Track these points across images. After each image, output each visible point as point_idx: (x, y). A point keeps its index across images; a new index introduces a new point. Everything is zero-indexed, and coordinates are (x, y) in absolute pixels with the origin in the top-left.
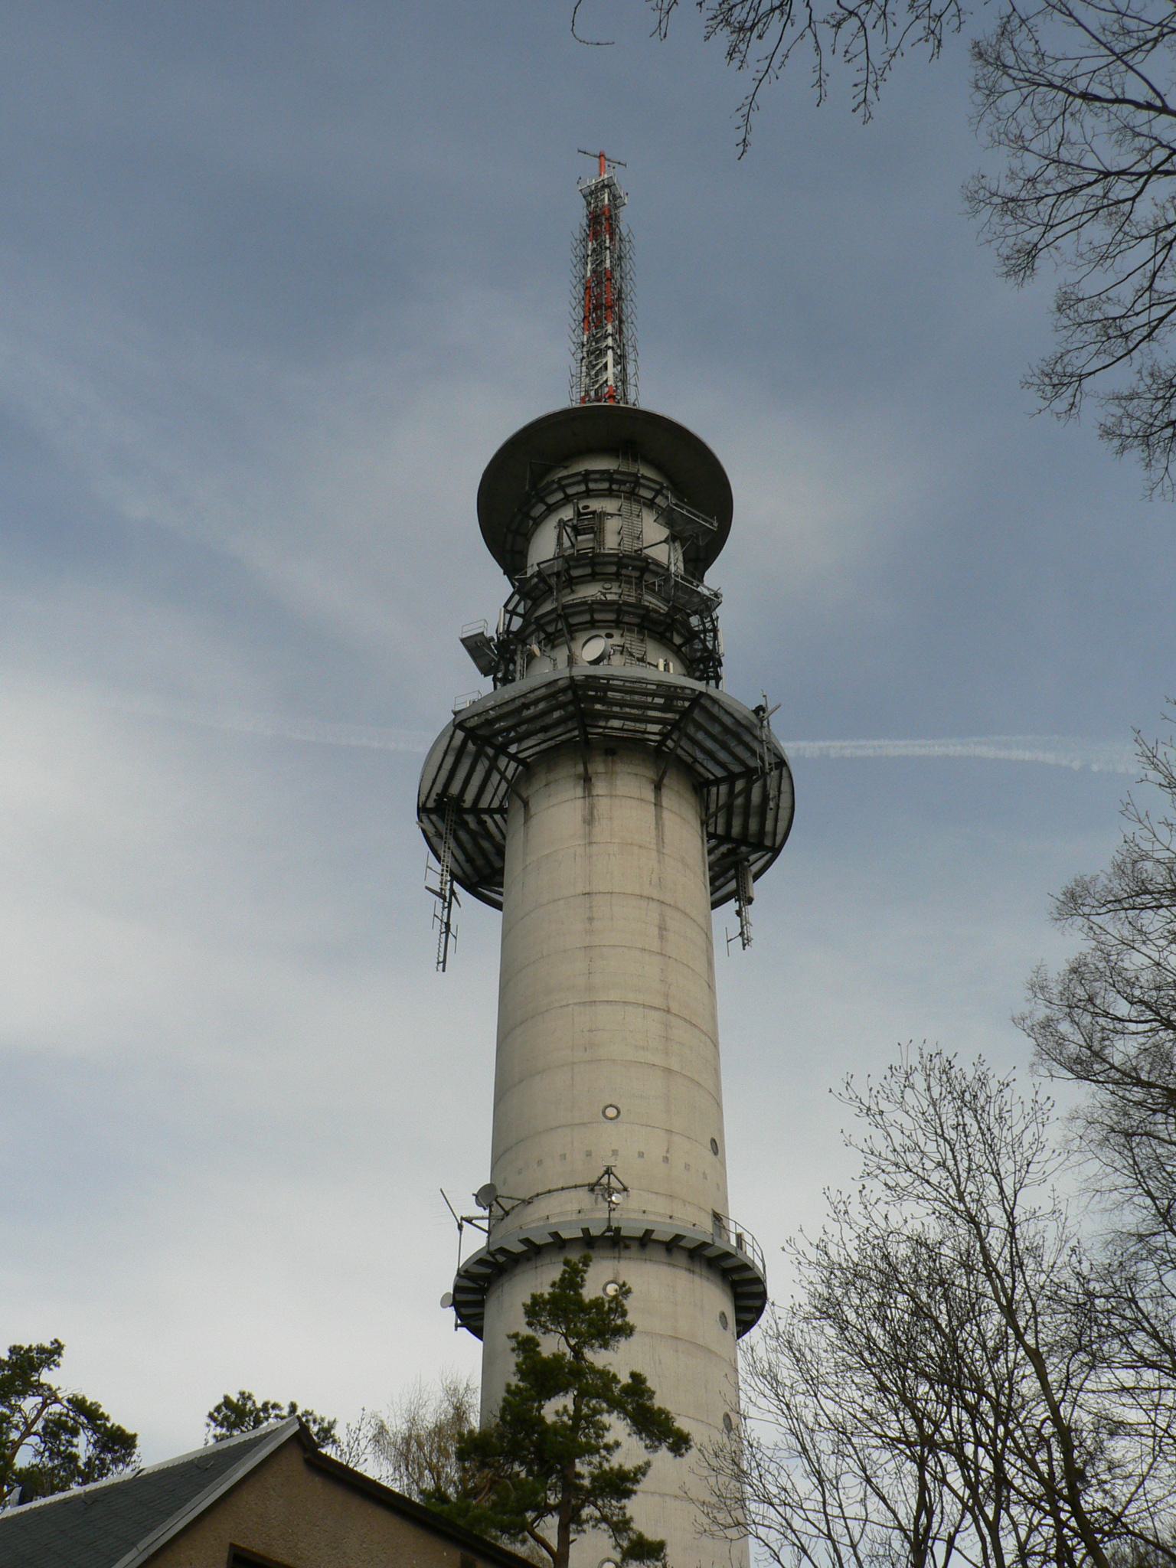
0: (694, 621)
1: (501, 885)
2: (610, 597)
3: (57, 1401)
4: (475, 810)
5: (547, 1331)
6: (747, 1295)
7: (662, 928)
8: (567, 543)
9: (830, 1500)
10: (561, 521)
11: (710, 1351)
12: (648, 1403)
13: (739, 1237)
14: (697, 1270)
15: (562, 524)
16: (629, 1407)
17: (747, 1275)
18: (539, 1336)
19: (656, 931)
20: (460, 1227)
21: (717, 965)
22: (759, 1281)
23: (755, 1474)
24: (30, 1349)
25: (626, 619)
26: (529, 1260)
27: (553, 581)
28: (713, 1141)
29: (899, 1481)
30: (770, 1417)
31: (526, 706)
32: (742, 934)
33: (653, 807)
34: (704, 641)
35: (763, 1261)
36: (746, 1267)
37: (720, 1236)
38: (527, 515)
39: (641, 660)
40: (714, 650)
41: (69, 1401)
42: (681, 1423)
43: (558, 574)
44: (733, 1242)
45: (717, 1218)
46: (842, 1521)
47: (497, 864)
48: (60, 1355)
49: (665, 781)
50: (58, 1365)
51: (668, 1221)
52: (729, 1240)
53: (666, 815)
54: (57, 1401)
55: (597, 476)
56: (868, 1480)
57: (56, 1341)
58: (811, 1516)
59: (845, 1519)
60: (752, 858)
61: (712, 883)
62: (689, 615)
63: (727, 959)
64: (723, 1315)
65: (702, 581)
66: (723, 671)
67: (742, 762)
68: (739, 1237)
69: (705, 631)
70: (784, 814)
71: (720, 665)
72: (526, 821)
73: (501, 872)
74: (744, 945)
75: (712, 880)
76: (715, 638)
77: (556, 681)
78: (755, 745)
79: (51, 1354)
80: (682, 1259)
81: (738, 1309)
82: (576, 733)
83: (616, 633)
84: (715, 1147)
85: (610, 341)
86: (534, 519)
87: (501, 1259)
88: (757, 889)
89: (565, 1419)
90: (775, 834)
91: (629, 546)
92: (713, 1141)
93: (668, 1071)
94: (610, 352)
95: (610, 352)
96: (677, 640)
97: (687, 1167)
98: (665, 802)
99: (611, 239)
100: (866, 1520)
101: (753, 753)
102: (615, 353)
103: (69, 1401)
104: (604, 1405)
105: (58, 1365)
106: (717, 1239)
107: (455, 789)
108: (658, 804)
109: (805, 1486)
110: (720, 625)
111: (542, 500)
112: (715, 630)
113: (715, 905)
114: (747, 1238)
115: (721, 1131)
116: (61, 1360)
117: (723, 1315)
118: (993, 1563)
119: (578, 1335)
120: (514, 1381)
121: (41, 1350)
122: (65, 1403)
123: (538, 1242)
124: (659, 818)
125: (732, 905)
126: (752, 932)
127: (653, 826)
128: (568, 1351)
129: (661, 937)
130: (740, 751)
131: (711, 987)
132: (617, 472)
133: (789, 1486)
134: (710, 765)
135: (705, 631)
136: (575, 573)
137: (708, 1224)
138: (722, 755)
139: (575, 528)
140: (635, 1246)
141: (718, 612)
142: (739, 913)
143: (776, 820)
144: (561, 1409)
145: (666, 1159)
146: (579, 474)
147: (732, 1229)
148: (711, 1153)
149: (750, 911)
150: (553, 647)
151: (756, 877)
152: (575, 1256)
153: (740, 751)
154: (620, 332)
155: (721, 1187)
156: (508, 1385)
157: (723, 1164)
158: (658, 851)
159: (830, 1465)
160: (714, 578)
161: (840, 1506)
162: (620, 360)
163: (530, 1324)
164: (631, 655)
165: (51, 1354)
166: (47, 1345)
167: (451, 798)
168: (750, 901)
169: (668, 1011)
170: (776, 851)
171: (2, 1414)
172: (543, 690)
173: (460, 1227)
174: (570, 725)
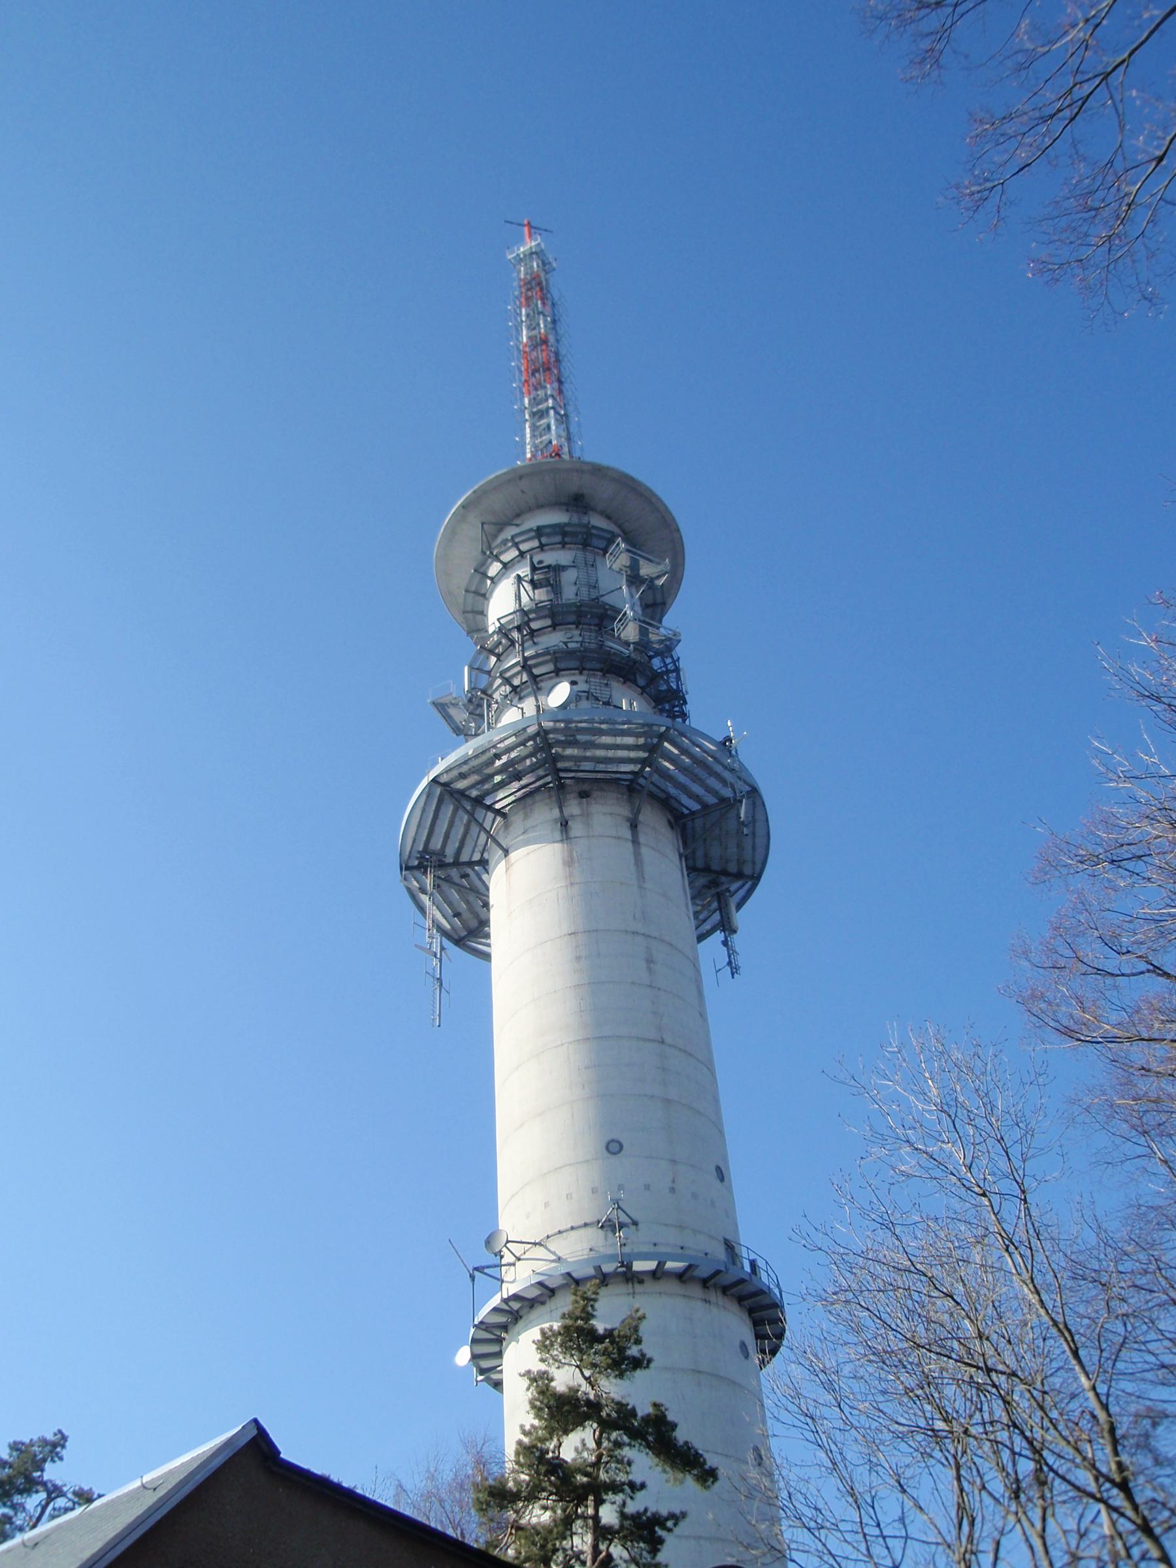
0: (656, 663)
1: (488, 936)
2: (571, 645)
3: (62, 1494)
4: (457, 863)
5: (561, 1365)
6: (764, 1317)
7: (650, 961)
8: (525, 599)
9: (866, 1519)
10: (518, 576)
11: (734, 1383)
12: (695, 1472)
13: (753, 1264)
14: (713, 1299)
15: (519, 579)
16: (650, 1438)
17: (767, 1301)
18: (553, 1371)
19: (644, 964)
20: (473, 1278)
21: (706, 992)
22: (777, 1306)
23: (784, 1494)
24: (32, 1444)
25: (588, 665)
26: (543, 1303)
27: (515, 635)
28: (718, 1169)
29: (936, 1486)
30: (795, 1432)
31: (498, 756)
32: (730, 963)
33: (630, 844)
34: (667, 682)
35: (778, 1286)
36: (762, 1292)
37: (734, 1263)
38: (485, 575)
39: (607, 703)
40: (679, 690)
41: (75, 1493)
42: (711, 1461)
43: (519, 628)
44: (747, 1268)
45: (730, 1247)
46: (881, 1539)
47: (483, 917)
48: (63, 1447)
49: (641, 818)
50: (61, 1459)
51: (680, 1251)
52: (743, 1268)
53: (644, 850)
54: (62, 1494)
55: (548, 530)
56: (904, 1491)
57: (60, 1432)
58: (848, 1537)
59: (884, 1538)
60: (733, 887)
61: (696, 918)
62: (651, 658)
63: (719, 993)
64: (743, 1346)
65: (660, 621)
66: (688, 708)
67: (715, 793)
68: (753, 1264)
69: (668, 672)
70: (760, 842)
71: (685, 702)
72: (507, 869)
73: (485, 923)
74: (733, 974)
75: (696, 914)
76: (678, 678)
77: (524, 729)
78: (727, 775)
79: (55, 1447)
80: (697, 1291)
81: (759, 1336)
82: (549, 779)
83: (580, 679)
84: (721, 1175)
85: (550, 402)
86: (492, 579)
87: (515, 1305)
88: (740, 918)
89: (585, 1454)
90: (754, 863)
91: (585, 594)
92: (718, 1169)
93: (667, 1101)
94: (552, 412)
95: (552, 412)
96: (641, 682)
97: (695, 1196)
98: (642, 839)
99: (544, 304)
100: (907, 1537)
101: (724, 782)
102: (557, 413)
103: (75, 1493)
104: (626, 1439)
105: (61, 1459)
106: (731, 1267)
107: (436, 844)
108: (635, 841)
109: (842, 1510)
110: (682, 665)
111: (497, 558)
112: (677, 670)
113: (701, 938)
114: (761, 1263)
115: (725, 1158)
116: (64, 1453)
117: (743, 1346)
118: (1045, 1564)
119: (594, 1365)
120: (530, 1420)
121: (44, 1442)
122: (70, 1496)
123: (551, 1286)
124: (637, 855)
125: (719, 936)
126: (740, 961)
127: (633, 862)
128: (583, 1382)
129: (650, 969)
130: (712, 782)
131: (703, 1015)
132: (566, 525)
133: (820, 1505)
134: (685, 800)
135: (668, 672)
136: (535, 625)
137: (720, 1253)
138: (696, 789)
139: (532, 582)
140: (647, 1279)
141: (679, 651)
142: (725, 943)
143: (754, 848)
144: (579, 1445)
145: (672, 1190)
146: (531, 530)
147: (745, 1255)
148: (718, 1183)
149: (736, 939)
150: (521, 699)
151: (739, 906)
152: (588, 1288)
153: (712, 782)
154: (560, 392)
155: (730, 1213)
156: (522, 1427)
157: (729, 1189)
158: (640, 887)
159: (862, 1478)
160: (672, 620)
161: (878, 1525)
162: (564, 419)
163: (542, 1360)
164: (597, 699)
165: (55, 1447)
166: (50, 1437)
167: (432, 853)
168: (734, 931)
169: (663, 1042)
170: (756, 878)
171: (4, 1515)
172: (513, 739)
173: (473, 1278)
174: (541, 772)
